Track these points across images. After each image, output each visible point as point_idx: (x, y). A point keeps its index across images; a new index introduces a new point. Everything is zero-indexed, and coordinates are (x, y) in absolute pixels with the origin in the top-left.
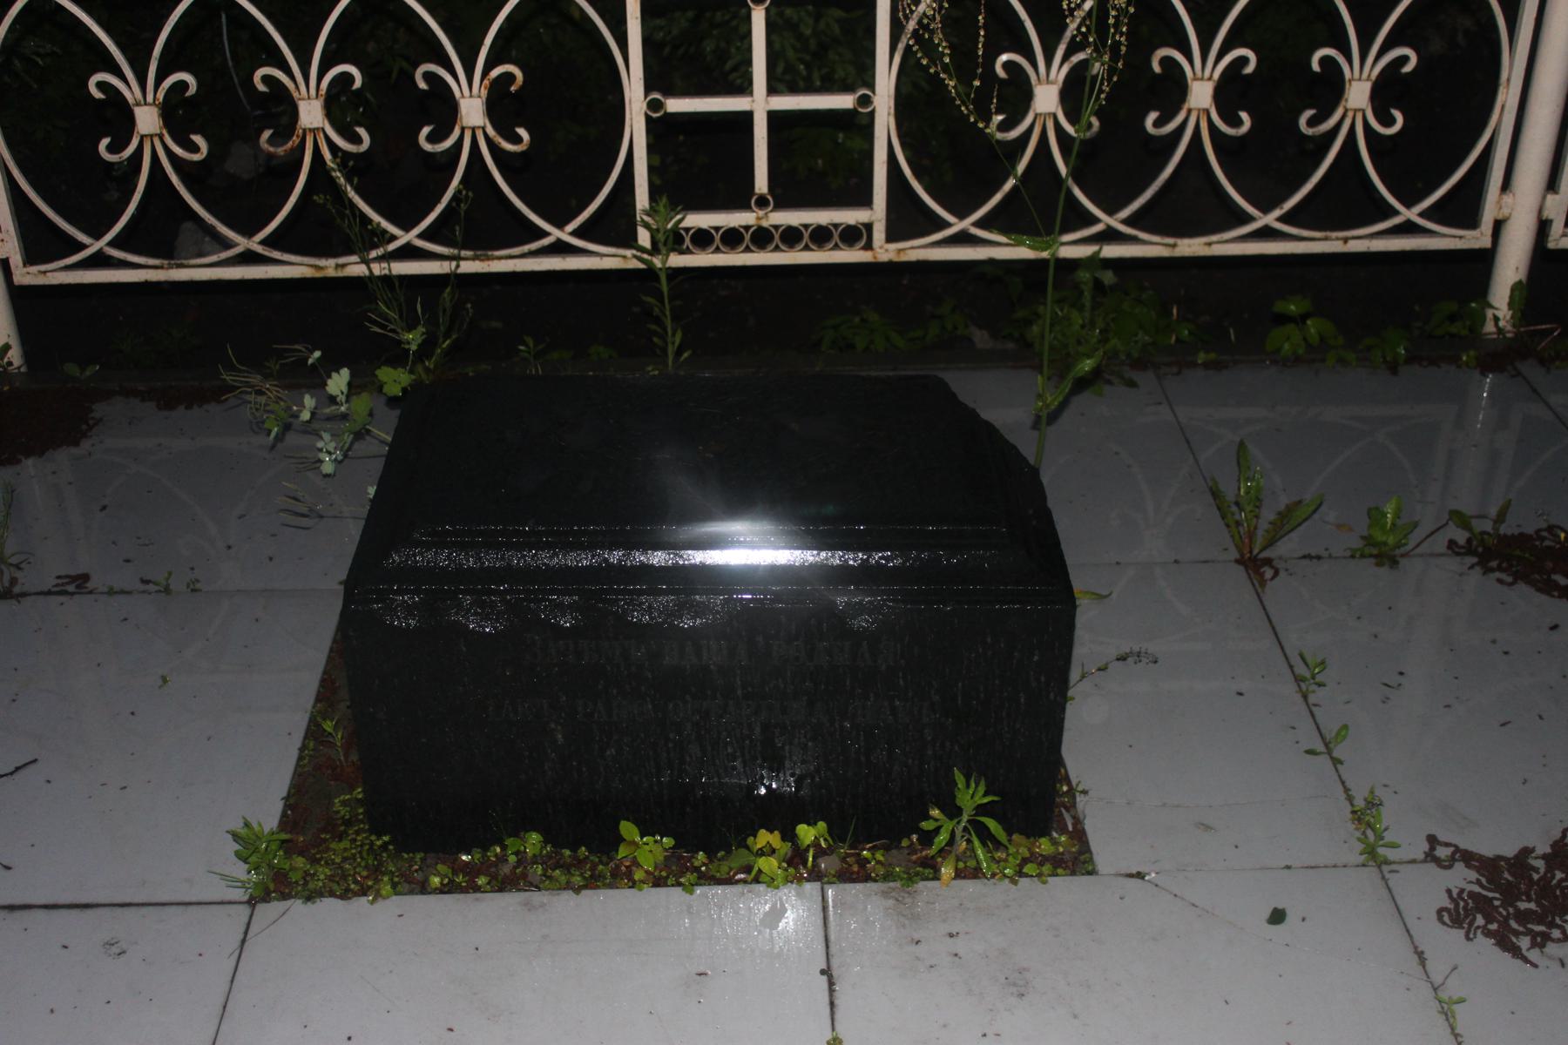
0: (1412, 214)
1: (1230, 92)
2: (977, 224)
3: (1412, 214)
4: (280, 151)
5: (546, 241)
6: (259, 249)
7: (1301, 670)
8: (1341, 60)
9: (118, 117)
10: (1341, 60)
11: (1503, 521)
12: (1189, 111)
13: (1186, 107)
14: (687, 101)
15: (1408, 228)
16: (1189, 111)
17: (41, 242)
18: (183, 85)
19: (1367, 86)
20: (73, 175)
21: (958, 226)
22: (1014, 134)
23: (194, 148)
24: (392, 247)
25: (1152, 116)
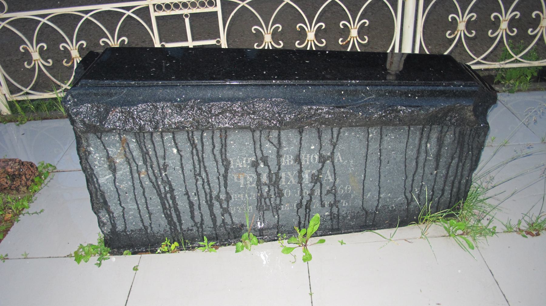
0: (517, 57)
1: (469, 25)
2: (521, 57)
3: (517, 57)
4: (70, 64)
5: (513, 59)
6: (480, 60)
7: (24, 257)
8: (499, 15)
9: (27, 56)
10: (499, 15)
11: (173, 190)
12: (308, 41)
13: (540, 26)
14: (183, 46)
15: (516, 61)
16: (308, 41)
17: (13, 90)
18: (83, 44)
19: (356, 30)
20: (19, 72)
21: (477, 59)
22: (452, 36)
23: (49, 63)
24: (513, 59)
25: (490, 31)
